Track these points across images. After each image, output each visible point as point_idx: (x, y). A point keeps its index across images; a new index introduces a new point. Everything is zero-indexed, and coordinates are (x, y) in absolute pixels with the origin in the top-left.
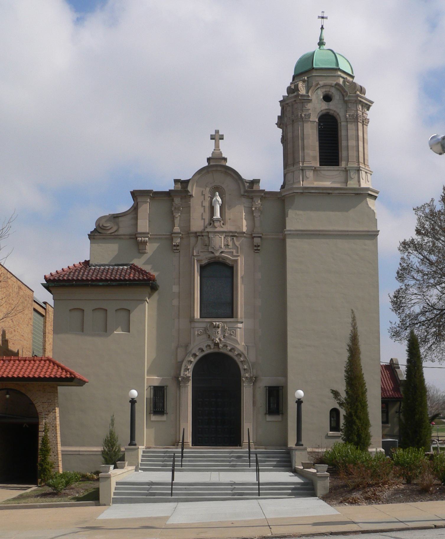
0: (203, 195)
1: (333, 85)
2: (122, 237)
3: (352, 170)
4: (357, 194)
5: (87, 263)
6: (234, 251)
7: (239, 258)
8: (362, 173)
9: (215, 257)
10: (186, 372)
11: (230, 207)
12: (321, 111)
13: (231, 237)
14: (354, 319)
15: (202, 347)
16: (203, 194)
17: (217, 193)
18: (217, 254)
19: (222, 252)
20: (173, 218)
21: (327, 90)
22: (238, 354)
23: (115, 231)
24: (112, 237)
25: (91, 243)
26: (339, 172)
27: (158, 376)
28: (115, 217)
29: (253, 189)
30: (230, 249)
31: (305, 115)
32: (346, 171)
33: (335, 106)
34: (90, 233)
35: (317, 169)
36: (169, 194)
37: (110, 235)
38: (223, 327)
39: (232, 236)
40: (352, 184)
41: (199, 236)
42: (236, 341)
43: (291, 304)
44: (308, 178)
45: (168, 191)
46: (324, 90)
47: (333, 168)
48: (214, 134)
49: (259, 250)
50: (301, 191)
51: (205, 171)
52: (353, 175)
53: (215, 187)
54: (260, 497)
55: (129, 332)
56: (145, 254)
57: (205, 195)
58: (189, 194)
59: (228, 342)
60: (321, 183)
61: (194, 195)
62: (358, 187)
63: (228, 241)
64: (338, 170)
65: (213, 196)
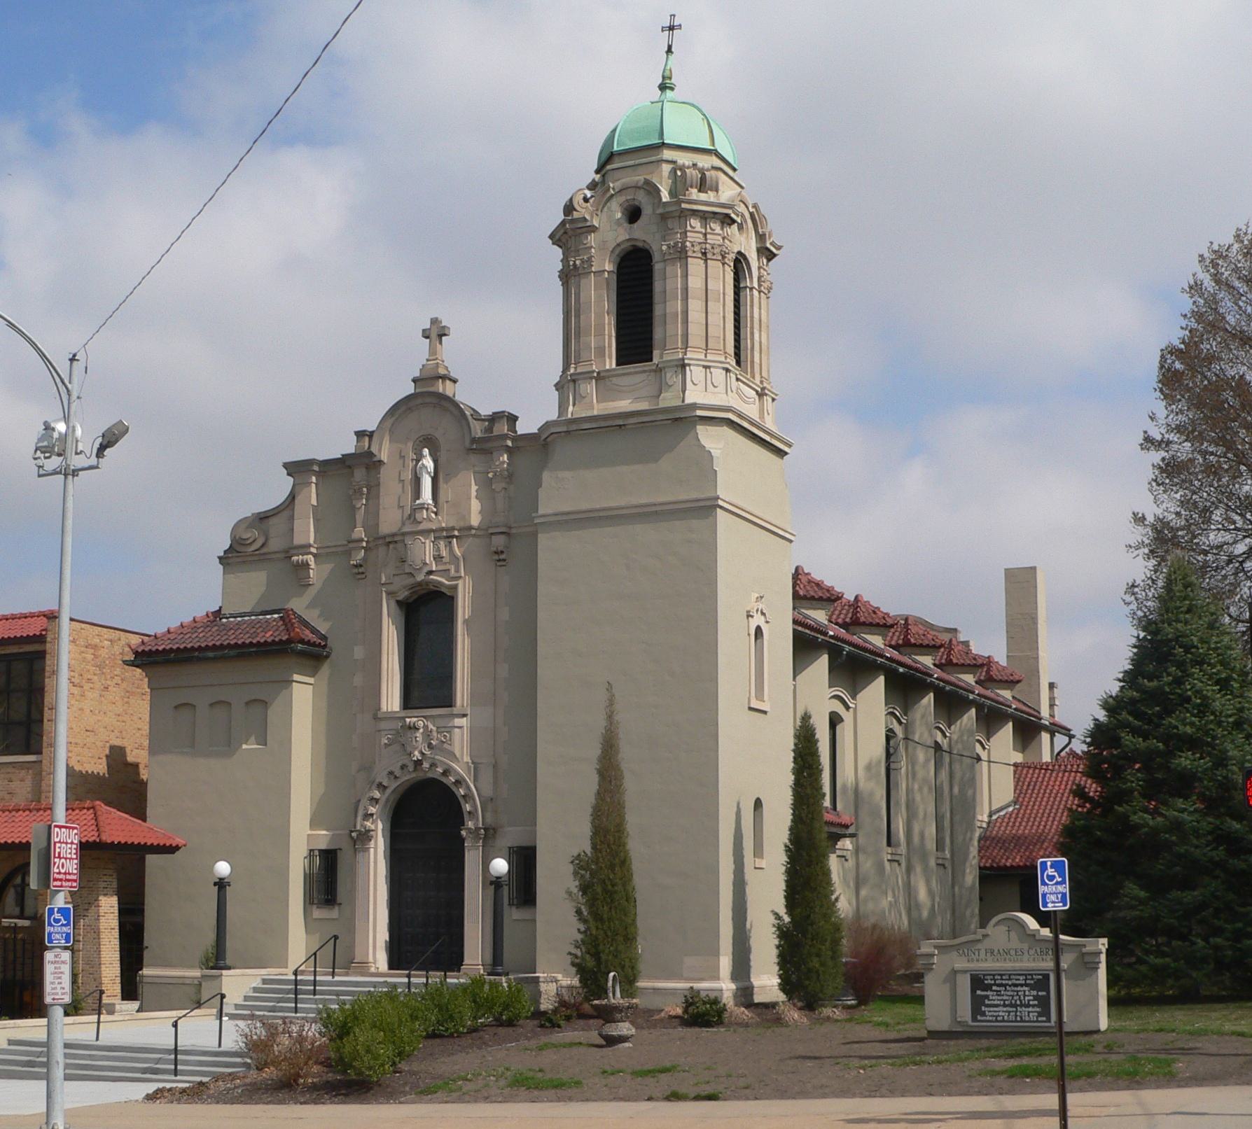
0: (403, 457)
1: (641, 184)
2: (273, 556)
3: (669, 367)
4: (676, 419)
5: (218, 614)
6: (453, 568)
7: (460, 582)
8: (691, 371)
9: (420, 584)
10: (367, 821)
11: (449, 477)
12: (618, 245)
13: (447, 540)
14: (611, 702)
15: (392, 769)
16: (402, 454)
17: (426, 451)
18: (420, 577)
19: (431, 572)
20: (354, 509)
21: (629, 198)
22: (456, 781)
23: (263, 545)
24: (256, 558)
25: (224, 574)
26: (645, 375)
27: (327, 830)
28: (263, 518)
29: (492, 433)
30: (446, 563)
31: (583, 261)
32: (659, 370)
33: (643, 232)
34: (222, 554)
35: (602, 375)
36: (345, 463)
37: (252, 555)
38: (426, 727)
39: (448, 537)
40: (668, 400)
41: (390, 542)
42: (452, 755)
43: (545, 672)
44: (584, 397)
45: (340, 456)
46: (622, 199)
47: (633, 367)
48: (429, 327)
49: (504, 560)
50: (565, 429)
51: (403, 408)
52: (671, 377)
53: (420, 441)
54: (179, 1078)
55: (266, 745)
56: (310, 587)
57: (404, 457)
58: (375, 459)
59: (437, 757)
60: (611, 403)
61: (385, 461)
62: (680, 404)
63: (438, 549)
64: (645, 372)
65: (419, 457)
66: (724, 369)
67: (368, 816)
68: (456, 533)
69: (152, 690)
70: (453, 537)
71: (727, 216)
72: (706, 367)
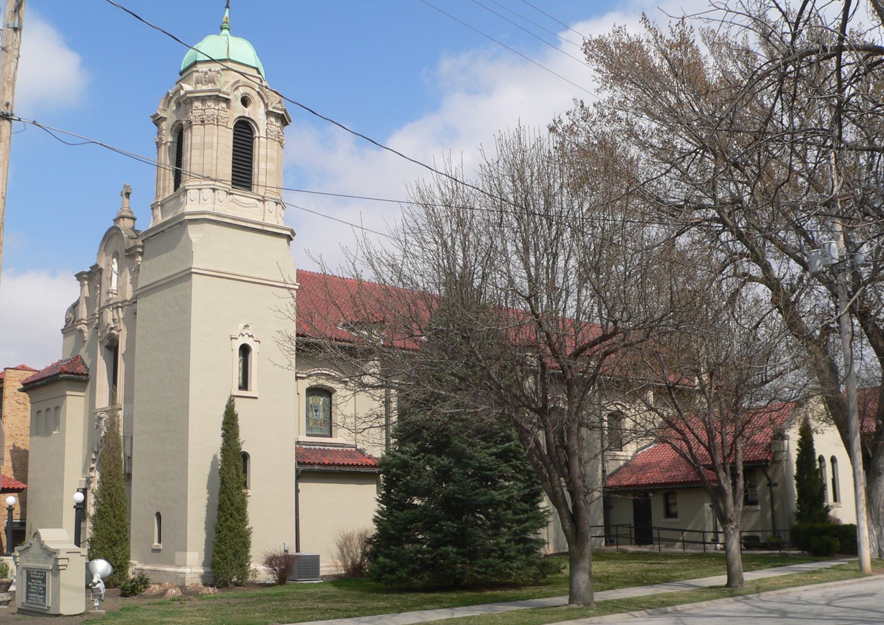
66: (211, 188)
67: (92, 469)
68: (120, 305)
69: (32, 404)
70: (118, 307)
71: (217, 96)
72: (200, 189)
